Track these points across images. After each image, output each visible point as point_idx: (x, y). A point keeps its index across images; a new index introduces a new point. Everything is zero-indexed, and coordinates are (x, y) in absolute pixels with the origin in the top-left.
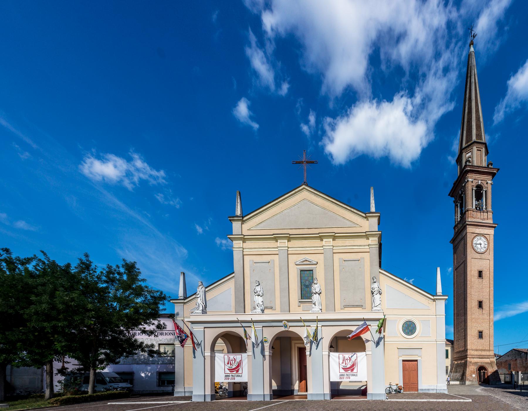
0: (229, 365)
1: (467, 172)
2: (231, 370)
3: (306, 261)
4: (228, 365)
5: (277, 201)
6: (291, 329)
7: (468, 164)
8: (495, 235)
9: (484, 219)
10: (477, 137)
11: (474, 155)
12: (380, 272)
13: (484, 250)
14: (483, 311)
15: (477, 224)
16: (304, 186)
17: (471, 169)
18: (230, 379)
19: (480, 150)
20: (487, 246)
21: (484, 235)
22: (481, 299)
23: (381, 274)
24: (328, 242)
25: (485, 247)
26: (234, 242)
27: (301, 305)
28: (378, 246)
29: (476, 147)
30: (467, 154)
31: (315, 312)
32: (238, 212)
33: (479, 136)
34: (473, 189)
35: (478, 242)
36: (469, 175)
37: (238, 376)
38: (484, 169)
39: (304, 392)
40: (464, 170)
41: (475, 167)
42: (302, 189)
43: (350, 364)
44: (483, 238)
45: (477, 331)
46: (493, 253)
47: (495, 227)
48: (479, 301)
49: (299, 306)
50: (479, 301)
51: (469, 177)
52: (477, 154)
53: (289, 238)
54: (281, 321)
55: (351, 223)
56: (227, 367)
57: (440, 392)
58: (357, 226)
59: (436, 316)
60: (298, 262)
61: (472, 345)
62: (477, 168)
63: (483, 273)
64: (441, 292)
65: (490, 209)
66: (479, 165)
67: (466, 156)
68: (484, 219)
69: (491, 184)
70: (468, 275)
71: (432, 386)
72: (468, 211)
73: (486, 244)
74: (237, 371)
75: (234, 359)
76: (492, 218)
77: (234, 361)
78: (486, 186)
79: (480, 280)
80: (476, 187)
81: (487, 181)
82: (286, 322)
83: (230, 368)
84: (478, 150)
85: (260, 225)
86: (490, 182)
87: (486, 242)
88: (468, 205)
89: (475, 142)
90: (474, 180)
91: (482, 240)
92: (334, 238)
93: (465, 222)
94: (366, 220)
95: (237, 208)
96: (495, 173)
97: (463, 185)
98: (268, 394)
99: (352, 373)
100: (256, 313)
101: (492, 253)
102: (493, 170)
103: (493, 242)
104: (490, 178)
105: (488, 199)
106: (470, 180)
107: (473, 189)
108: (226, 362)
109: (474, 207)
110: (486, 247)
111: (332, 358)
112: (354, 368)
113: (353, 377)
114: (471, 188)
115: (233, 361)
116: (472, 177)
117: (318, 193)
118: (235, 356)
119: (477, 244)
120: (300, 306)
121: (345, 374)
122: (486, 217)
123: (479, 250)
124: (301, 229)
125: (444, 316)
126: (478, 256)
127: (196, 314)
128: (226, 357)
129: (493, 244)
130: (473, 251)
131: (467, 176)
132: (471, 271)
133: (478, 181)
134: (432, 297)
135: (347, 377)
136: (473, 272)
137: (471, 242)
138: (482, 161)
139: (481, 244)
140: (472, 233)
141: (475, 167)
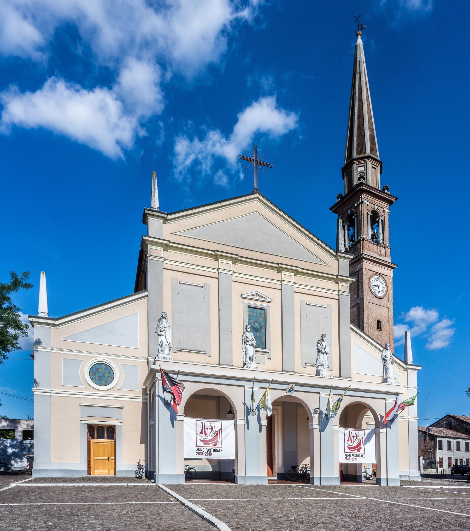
0: (349, 442)
1: (362, 191)
2: (351, 448)
3: (257, 295)
4: (201, 435)
5: (219, 205)
6: (294, 394)
8: (394, 278)
9: (381, 255)
10: (371, 151)
11: (369, 172)
12: (351, 329)
13: (383, 295)
15: (375, 260)
16: (257, 195)
17: (367, 189)
18: (351, 460)
19: (375, 168)
21: (381, 275)
23: (351, 331)
24: (287, 276)
25: (383, 291)
28: (349, 295)
29: (370, 163)
30: (359, 167)
31: (326, 377)
32: (156, 203)
33: (373, 149)
35: (376, 284)
36: (364, 196)
37: (360, 456)
38: (382, 193)
39: (271, 476)
40: (359, 187)
41: (372, 189)
42: (254, 198)
43: (212, 435)
44: (380, 278)
46: (392, 301)
47: (393, 268)
51: (364, 198)
52: (371, 171)
53: (236, 260)
54: (288, 383)
55: (316, 259)
56: (199, 438)
57: (413, 480)
58: (324, 264)
59: (407, 388)
60: (246, 295)
62: (374, 190)
63: (382, 324)
64: (412, 361)
65: (387, 244)
66: (374, 186)
69: (388, 214)
71: (404, 471)
72: (363, 240)
73: (384, 288)
74: (359, 450)
75: (211, 428)
76: (390, 255)
77: (211, 429)
78: (383, 214)
81: (384, 208)
82: (294, 385)
83: (203, 438)
84: (372, 167)
85: (191, 231)
86: (387, 210)
87: (384, 285)
88: (363, 233)
89: (369, 157)
90: (370, 203)
92: (297, 273)
94: (335, 259)
95: (154, 196)
96: (393, 201)
97: (356, 205)
98: (385, 478)
99: (359, 454)
100: (252, 369)
101: (391, 299)
102: (392, 198)
103: (392, 286)
104: (387, 206)
105: (385, 231)
106: (365, 202)
107: (368, 214)
108: (199, 430)
109: (370, 238)
110: (385, 291)
111: (186, 423)
112: (360, 448)
113: (359, 458)
115: (210, 430)
117: (277, 210)
118: (212, 422)
119: (374, 286)
121: (351, 454)
122: (383, 253)
123: (376, 294)
124: (250, 250)
125: (416, 389)
127: (164, 360)
128: (199, 423)
129: (392, 289)
130: (370, 293)
131: (361, 195)
132: (368, 319)
133: (373, 206)
134: (405, 366)
135: (207, 452)
136: (370, 320)
138: (377, 182)
139: (378, 286)
140: (368, 270)
141: (372, 189)
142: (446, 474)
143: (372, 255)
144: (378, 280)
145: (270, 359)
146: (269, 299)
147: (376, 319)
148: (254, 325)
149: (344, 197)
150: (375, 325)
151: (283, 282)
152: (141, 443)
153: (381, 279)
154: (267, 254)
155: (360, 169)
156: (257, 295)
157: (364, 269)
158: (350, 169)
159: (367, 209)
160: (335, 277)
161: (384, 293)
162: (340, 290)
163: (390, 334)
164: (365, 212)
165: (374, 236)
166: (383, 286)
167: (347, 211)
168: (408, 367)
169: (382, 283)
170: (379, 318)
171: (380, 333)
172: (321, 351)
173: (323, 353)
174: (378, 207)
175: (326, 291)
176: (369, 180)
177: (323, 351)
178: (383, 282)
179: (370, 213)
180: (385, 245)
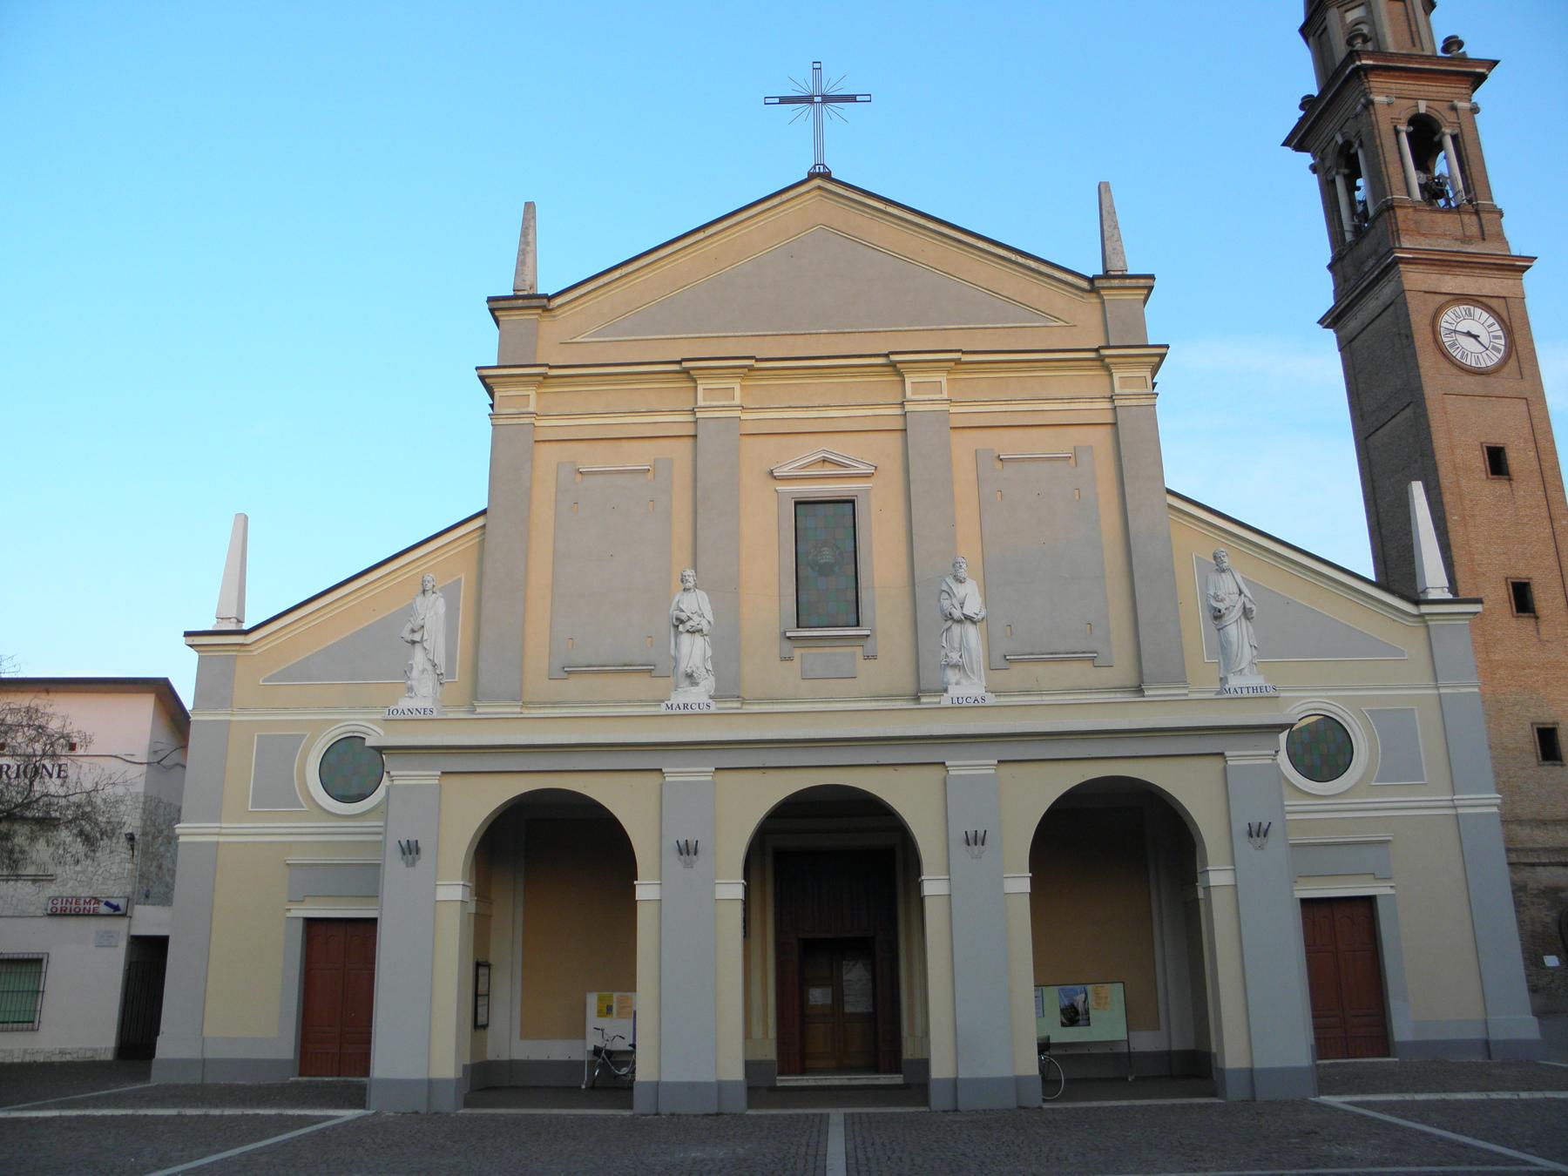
1: (1362, 73)
7: (1358, 44)
12: (1171, 506)
13: (1496, 360)
14: (1543, 629)
20: (1502, 342)
22: (1521, 573)
23: (1173, 516)
26: (501, 394)
27: (797, 653)
34: (1397, 133)
45: (1528, 727)
48: (1513, 584)
49: (784, 659)
50: (1513, 584)
61: (1517, 798)
67: (1343, 18)
68: (1466, 239)
70: (1439, 465)
79: (1501, 486)
80: (1411, 122)
81: (1452, 101)
87: (1497, 327)
91: (1476, 318)
93: (1391, 251)
109: (1417, 194)
114: (1391, 126)
116: (1385, 90)
120: (790, 659)
122: (1474, 230)
123: (1470, 362)
126: (1470, 383)
130: (1443, 364)
133: (1412, 103)
137: (1429, 329)
138: (1416, 37)
142: (1132, 1050)
143: (1431, 245)
144: (1471, 316)
145: (874, 657)
146: (862, 467)
147: (1482, 444)
148: (816, 555)
149: (1318, 96)
150: (1482, 466)
151: (909, 407)
152: (1298, 140)
153: (1478, 311)
154: (855, 332)
155: (1351, 16)
156: (824, 461)
157: (1408, 295)
158: (1324, 24)
159: (1392, 118)
160: (1092, 355)
161: (1500, 356)
162: (1117, 391)
163: (1547, 486)
164: (1385, 127)
165: (1433, 191)
166: (1491, 334)
167: (1334, 137)
168: (1425, 609)
169: (1486, 325)
170: (1495, 440)
171: (1507, 487)
172: (950, 614)
173: (959, 621)
174: (1431, 104)
175: (1066, 406)
176: (1384, 36)
177: (957, 614)
178: (1491, 320)
179: (1403, 128)
180: (1475, 208)
